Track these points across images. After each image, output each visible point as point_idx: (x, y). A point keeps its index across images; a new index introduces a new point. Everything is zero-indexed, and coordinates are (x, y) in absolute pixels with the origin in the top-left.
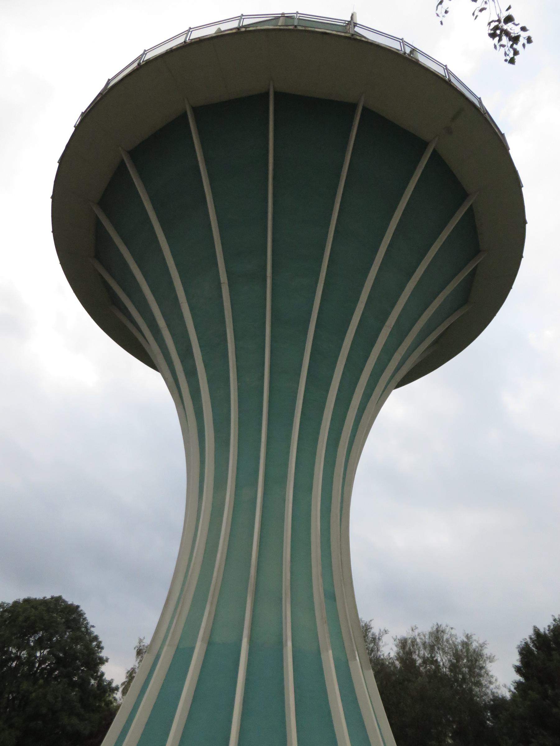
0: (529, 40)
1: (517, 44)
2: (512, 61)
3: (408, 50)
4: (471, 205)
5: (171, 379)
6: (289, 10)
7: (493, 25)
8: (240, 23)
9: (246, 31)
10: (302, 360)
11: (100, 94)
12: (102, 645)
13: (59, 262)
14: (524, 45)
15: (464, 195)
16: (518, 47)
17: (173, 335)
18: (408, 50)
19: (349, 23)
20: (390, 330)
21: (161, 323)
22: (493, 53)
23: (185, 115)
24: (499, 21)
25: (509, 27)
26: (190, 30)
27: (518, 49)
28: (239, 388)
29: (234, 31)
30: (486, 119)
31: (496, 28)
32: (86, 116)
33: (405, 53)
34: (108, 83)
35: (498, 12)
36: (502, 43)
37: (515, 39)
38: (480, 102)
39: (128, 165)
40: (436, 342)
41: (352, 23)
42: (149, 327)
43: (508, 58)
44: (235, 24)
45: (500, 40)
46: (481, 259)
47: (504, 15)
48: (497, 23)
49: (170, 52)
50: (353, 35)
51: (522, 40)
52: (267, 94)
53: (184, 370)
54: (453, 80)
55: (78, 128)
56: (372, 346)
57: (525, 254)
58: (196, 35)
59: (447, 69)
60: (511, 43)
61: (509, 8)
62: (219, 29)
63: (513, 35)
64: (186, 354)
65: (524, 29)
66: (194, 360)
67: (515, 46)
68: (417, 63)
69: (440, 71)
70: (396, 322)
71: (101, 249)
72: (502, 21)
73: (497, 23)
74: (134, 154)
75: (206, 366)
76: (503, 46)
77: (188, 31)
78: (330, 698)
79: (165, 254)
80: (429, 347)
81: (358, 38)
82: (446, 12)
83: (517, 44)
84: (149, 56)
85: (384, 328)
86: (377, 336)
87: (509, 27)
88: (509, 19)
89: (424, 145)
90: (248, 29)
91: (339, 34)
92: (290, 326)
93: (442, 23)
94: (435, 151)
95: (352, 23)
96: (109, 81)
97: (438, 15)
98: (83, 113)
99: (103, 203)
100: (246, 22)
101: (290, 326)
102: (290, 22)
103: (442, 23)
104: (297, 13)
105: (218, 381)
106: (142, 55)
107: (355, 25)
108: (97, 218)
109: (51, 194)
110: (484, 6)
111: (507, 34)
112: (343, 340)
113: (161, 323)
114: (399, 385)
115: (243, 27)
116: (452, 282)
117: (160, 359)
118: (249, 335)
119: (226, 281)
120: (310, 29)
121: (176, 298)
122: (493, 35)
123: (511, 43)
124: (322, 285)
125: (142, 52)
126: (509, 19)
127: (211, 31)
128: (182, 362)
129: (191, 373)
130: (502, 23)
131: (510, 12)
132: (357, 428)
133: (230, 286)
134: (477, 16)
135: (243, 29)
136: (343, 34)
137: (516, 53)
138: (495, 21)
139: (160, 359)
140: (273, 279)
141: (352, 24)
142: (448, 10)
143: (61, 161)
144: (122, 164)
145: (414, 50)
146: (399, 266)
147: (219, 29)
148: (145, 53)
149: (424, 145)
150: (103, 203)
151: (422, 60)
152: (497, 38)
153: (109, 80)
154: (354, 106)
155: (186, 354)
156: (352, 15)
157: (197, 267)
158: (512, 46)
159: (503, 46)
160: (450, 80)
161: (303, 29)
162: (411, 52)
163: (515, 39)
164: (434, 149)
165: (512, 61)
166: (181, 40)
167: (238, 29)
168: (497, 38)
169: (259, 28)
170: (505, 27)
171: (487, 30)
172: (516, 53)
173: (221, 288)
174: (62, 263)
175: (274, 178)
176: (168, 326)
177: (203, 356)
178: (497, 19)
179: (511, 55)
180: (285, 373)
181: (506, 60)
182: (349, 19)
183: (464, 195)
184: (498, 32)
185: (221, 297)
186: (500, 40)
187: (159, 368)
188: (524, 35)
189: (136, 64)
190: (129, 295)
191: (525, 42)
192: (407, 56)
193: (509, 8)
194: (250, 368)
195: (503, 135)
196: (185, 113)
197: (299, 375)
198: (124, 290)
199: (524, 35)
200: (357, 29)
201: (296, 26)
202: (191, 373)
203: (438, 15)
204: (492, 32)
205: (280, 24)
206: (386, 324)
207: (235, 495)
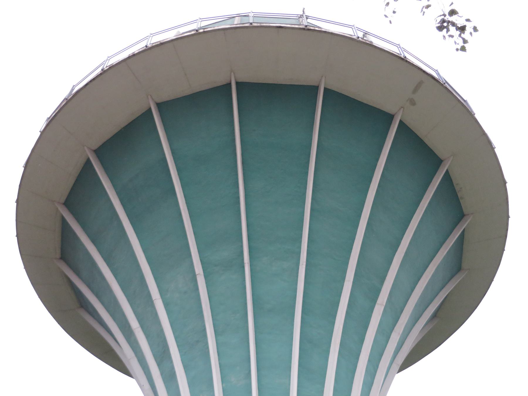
0: (475, 29)
1: (464, 33)
2: (463, 49)
4: (447, 171)
5: (147, 386)
8: (198, 25)
13: (23, 267)
14: (471, 33)
15: (438, 162)
16: (466, 35)
17: (147, 336)
18: (361, 35)
19: (301, 16)
25: (453, 19)
27: (466, 39)
29: (193, 33)
31: (443, 21)
33: (358, 37)
34: (72, 90)
36: (449, 33)
37: (462, 29)
38: (438, 74)
40: (435, 315)
45: (448, 30)
46: (467, 223)
48: (443, 17)
50: (306, 26)
51: (469, 29)
52: (229, 84)
59: (400, 47)
60: (458, 32)
61: (452, 4)
62: (179, 32)
63: (459, 26)
64: (163, 356)
65: (468, 20)
66: (172, 362)
67: (462, 35)
70: (388, 299)
71: (68, 249)
73: (443, 17)
74: (98, 152)
75: (186, 367)
76: (452, 36)
78: (174, 165)
81: (312, 28)
83: (464, 33)
86: (370, 316)
87: (453, 19)
88: (453, 12)
89: (390, 117)
90: (206, 30)
91: (293, 26)
92: (273, 313)
93: (390, 22)
94: (401, 122)
99: (68, 203)
101: (273, 313)
102: (245, 20)
103: (390, 22)
110: (428, 3)
111: (453, 24)
112: (333, 323)
114: (400, 370)
116: (441, 250)
117: (133, 364)
118: (230, 328)
120: (265, 25)
122: (440, 28)
124: (304, 266)
125: (106, 59)
126: (453, 12)
127: (171, 35)
128: (159, 365)
130: (447, 16)
131: (453, 7)
133: (206, 277)
134: (424, 12)
135: (201, 31)
136: (297, 26)
137: (465, 41)
138: (441, 16)
139: (133, 364)
140: (251, 265)
141: (305, 17)
142: (395, 10)
144: (88, 162)
145: (366, 34)
146: (382, 243)
149: (390, 117)
150: (68, 203)
152: (445, 30)
153: (74, 86)
154: (316, 89)
155: (163, 356)
157: (169, 258)
158: (460, 35)
159: (452, 36)
160: (405, 57)
161: (259, 25)
162: (363, 35)
163: (462, 29)
164: (400, 120)
165: (463, 49)
170: (451, 19)
174: (25, 268)
175: (243, 163)
176: (142, 327)
177: (181, 356)
178: (442, 13)
179: (461, 44)
182: (301, 13)
184: (445, 24)
185: (197, 289)
187: (132, 372)
191: (472, 31)
192: (361, 40)
193: (452, 4)
196: (150, 110)
197: (289, 368)
201: (251, 24)
203: (386, 16)
204: (439, 25)
205: (236, 23)
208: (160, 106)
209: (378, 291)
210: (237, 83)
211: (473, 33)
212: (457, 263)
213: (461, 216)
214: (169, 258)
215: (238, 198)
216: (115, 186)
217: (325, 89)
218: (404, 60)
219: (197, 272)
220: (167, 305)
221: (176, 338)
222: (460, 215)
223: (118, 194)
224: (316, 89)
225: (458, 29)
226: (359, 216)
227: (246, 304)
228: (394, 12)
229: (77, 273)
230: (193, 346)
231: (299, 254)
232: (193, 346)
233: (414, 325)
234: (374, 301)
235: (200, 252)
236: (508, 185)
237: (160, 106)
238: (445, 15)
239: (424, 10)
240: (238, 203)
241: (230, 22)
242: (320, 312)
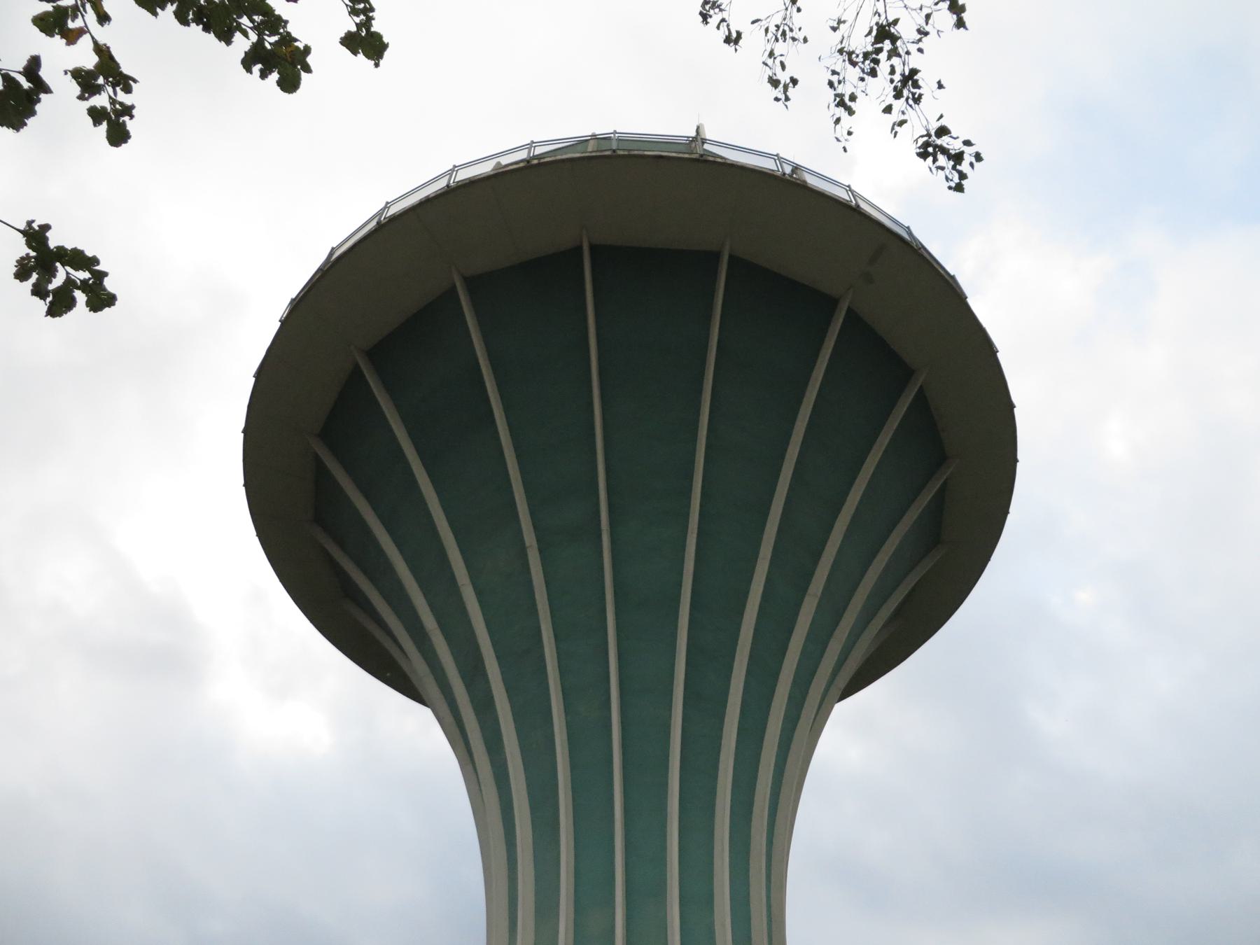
0: (978, 157)
2: (959, 188)
3: (788, 170)
5: (450, 719)
6: (602, 129)
7: (921, 141)
9: (539, 164)
10: (673, 665)
11: (319, 270)
12: (109, 284)
13: (254, 533)
14: (972, 165)
16: (964, 167)
18: (788, 170)
19: (694, 139)
20: (816, 601)
21: (429, 621)
22: (929, 179)
23: (452, 291)
24: (929, 135)
25: (944, 141)
26: (455, 169)
28: (569, 726)
29: (522, 165)
30: (921, 256)
31: (926, 145)
32: (297, 305)
34: (331, 254)
35: (925, 123)
36: (938, 164)
37: (958, 158)
39: (365, 372)
41: (698, 139)
42: (408, 630)
43: (953, 185)
44: (523, 155)
45: (935, 160)
47: (934, 126)
49: (427, 201)
51: (968, 159)
53: (472, 702)
54: (863, 206)
55: (285, 322)
56: (790, 632)
57: (1020, 456)
58: (463, 175)
60: (952, 163)
61: (941, 116)
62: (499, 163)
63: (953, 152)
65: (967, 143)
66: (487, 681)
68: (804, 187)
69: (843, 195)
72: (933, 133)
74: (379, 353)
75: (508, 690)
76: (942, 168)
77: (452, 170)
79: (465, 599)
80: (884, 626)
82: (850, 133)
84: (393, 210)
85: (807, 599)
87: (944, 141)
88: (942, 131)
89: (831, 303)
93: (845, 150)
94: (850, 311)
95: (698, 139)
96: (333, 250)
97: (838, 140)
98: (293, 300)
99: (325, 434)
100: (539, 151)
102: (605, 145)
103: (845, 150)
104: (615, 132)
105: (532, 717)
106: (383, 210)
107: (704, 141)
108: (317, 458)
109: (242, 425)
110: (902, 117)
111: (944, 151)
113: (429, 621)
115: (535, 157)
117: (418, 667)
118: (579, 631)
119: (535, 543)
121: (453, 579)
122: (923, 155)
123: (952, 163)
124: (695, 535)
125: (383, 205)
127: (486, 168)
129: (484, 707)
130: (934, 138)
131: (943, 122)
132: (781, 782)
133: (541, 551)
135: (535, 162)
137: (963, 176)
143: (259, 375)
144: (356, 373)
145: (796, 168)
147: (499, 163)
148: (387, 205)
149: (831, 303)
150: (325, 434)
151: (811, 181)
152: (930, 159)
154: (715, 256)
156: (698, 128)
157: (484, 523)
158: (954, 168)
159: (942, 168)
162: (793, 171)
163: (958, 158)
165: (959, 188)
166: (442, 184)
167: (527, 161)
168: (930, 159)
169: (559, 157)
170: (939, 142)
171: (913, 149)
172: (963, 176)
173: (526, 555)
177: (502, 673)
179: (956, 180)
180: (645, 692)
181: (950, 188)
182: (693, 134)
183: (904, 373)
184: (930, 150)
186: (935, 160)
187: (425, 697)
188: (968, 151)
189: (374, 223)
190: (373, 580)
191: (973, 160)
193: (941, 116)
194: (584, 690)
195: (953, 277)
198: (365, 571)
199: (968, 151)
200: (706, 146)
202: (484, 707)
203: (838, 140)
205: (590, 149)
206: (810, 591)
207: (576, 925)
208: (472, 283)
209: (808, 577)
210: (593, 248)
211: (976, 164)
212: (932, 532)
213: (941, 459)
214: (484, 523)
215: (592, 428)
216: (398, 407)
217: (731, 256)
218: (857, 210)
219: (527, 544)
220: (479, 593)
221: (495, 644)
222: (939, 457)
223: (405, 420)
224: (715, 256)
225: (950, 157)
226: (782, 457)
227: (604, 594)
228: (850, 133)
229: (341, 544)
230: (521, 659)
231: (687, 516)
232: (521, 659)
233: (868, 623)
234: (803, 590)
235: (532, 514)
236: (1016, 411)
237: (472, 283)
238: (929, 135)
239: (897, 128)
240: (593, 435)
241: (579, 148)
242: (718, 610)
